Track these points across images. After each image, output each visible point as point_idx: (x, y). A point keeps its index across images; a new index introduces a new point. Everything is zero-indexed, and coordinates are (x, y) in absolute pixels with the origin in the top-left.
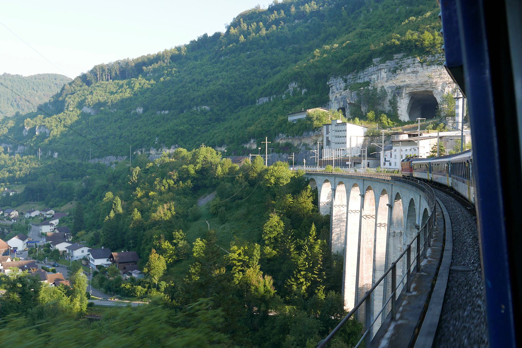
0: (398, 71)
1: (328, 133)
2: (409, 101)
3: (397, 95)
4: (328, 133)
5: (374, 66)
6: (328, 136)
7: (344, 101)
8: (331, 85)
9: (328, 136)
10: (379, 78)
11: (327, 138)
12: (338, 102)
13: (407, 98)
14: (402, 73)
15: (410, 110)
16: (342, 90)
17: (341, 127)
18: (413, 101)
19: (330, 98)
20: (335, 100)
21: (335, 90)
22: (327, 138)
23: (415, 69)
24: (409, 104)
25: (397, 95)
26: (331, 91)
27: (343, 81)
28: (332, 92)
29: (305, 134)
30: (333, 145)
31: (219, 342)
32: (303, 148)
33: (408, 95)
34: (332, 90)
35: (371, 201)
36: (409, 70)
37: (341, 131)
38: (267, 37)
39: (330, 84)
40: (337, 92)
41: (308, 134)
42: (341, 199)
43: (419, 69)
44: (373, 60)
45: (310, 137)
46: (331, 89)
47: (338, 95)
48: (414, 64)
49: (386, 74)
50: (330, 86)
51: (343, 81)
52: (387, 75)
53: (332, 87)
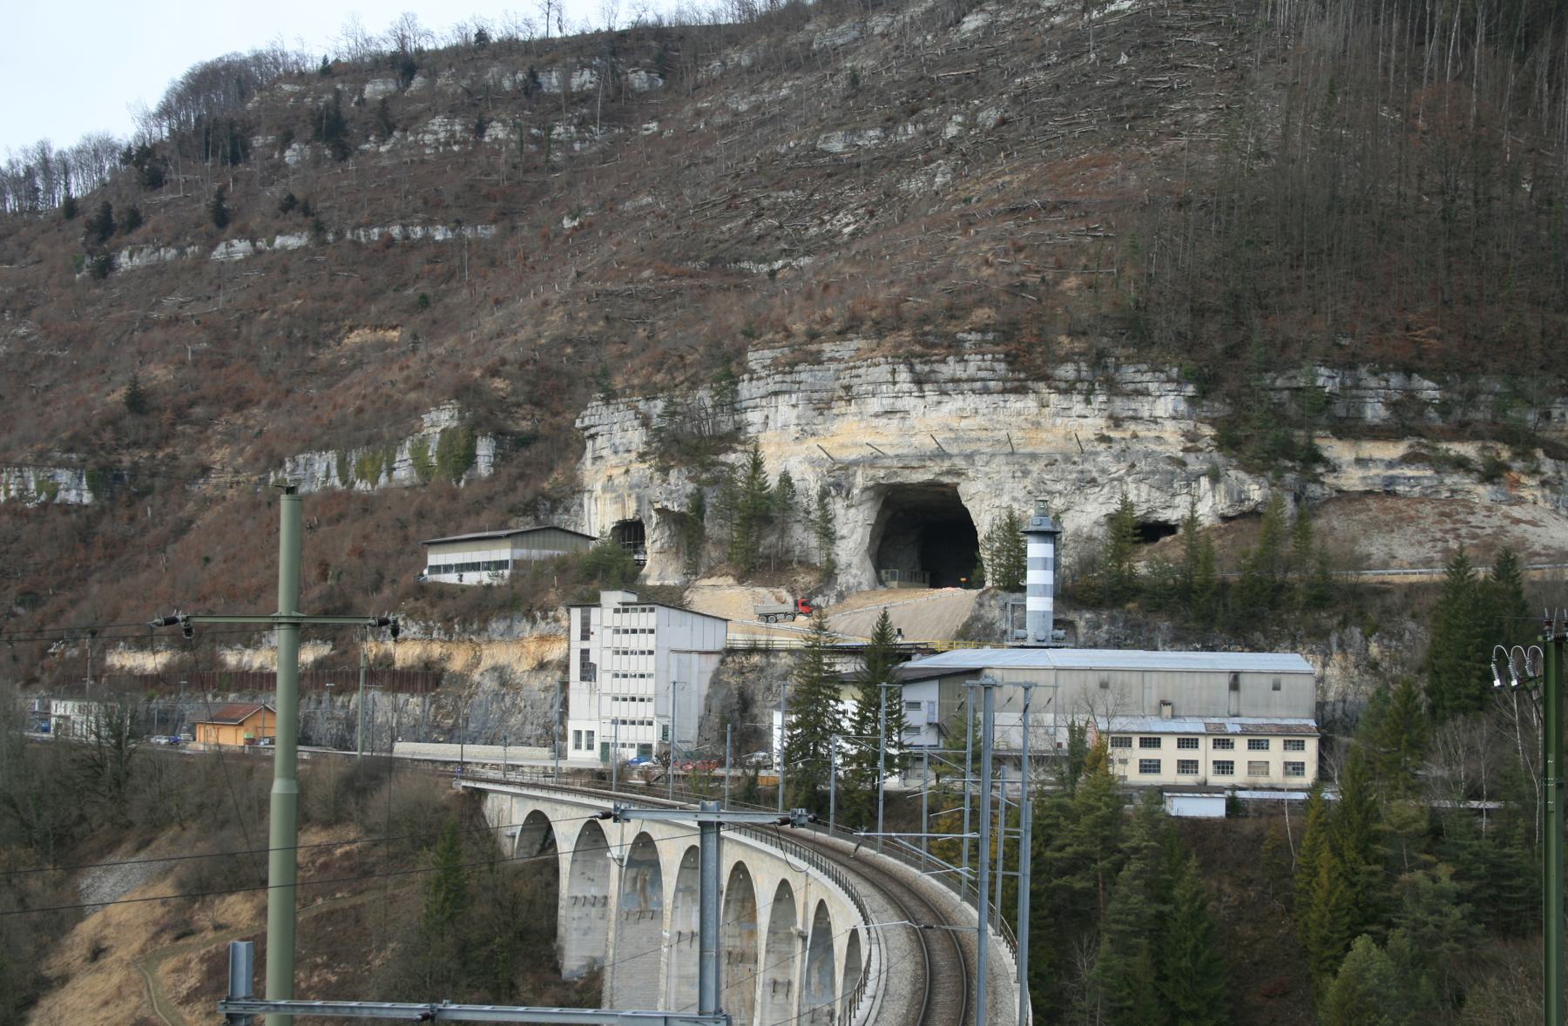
0: (839, 407)
1: (586, 634)
2: (874, 515)
3: (833, 492)
4: (586, 634)
5: (751, 379)
6: (585, 645)
7: (639, 499)
8: (593, 431)
9: (585, 645)
10: (771, 423)
11: (585, 653)
12: (620, 499)
13: (869, 504)
14: (855, 415)
15: (881, 546)
16: (633, 455)
17: (634, 615)
18: (889, 513)
19: (587, 480)
20: (604, 490)
21: (604, 453)
22: (585, 653)
23: (899, 404)
24: (875, 527)
25: (833, 492)
26: (589, 455)
27: (636, 423)
28: (596, 459)
29: (497, 626)
30: (604, 680)
31: (1563, 415)
32: (489, 683)
33: (872, 494)
34: (594, 451)
35: (743, 907)
36: (874, 405)
37: (634, 631)
38: (533, 548)
39: (586, 428)
40: (614, 460)
41: (510, 628)
42: (643, 889)
43: (907, 403)
44: (751, 356)
45: (519, 640)
46: (589, 444)
47: (615, 472)
48: (895, 383)
49: (795, 412)
50: (586, 434)
51: (636, 423)
52: (798, 417)
53: (593, 437)
